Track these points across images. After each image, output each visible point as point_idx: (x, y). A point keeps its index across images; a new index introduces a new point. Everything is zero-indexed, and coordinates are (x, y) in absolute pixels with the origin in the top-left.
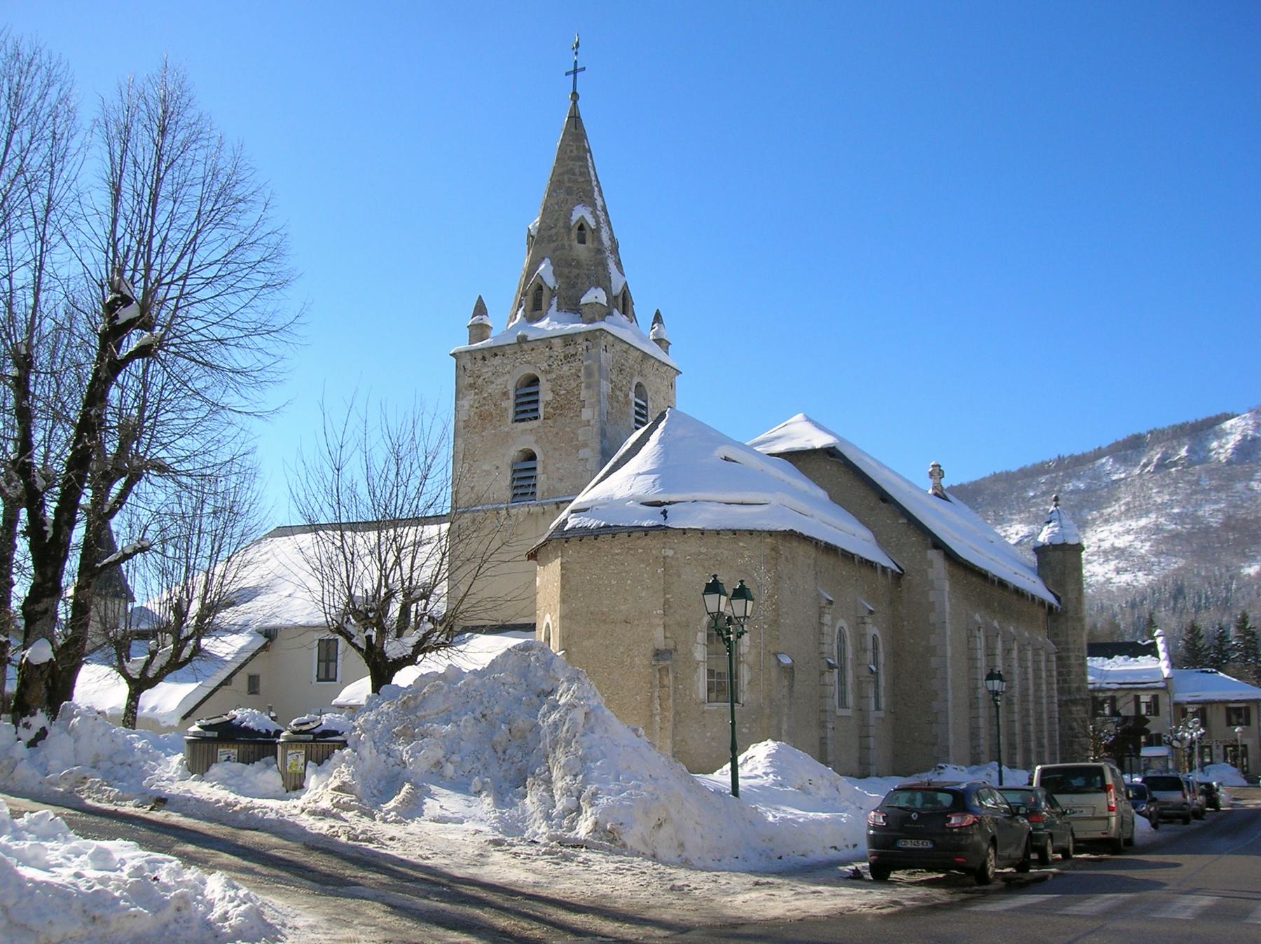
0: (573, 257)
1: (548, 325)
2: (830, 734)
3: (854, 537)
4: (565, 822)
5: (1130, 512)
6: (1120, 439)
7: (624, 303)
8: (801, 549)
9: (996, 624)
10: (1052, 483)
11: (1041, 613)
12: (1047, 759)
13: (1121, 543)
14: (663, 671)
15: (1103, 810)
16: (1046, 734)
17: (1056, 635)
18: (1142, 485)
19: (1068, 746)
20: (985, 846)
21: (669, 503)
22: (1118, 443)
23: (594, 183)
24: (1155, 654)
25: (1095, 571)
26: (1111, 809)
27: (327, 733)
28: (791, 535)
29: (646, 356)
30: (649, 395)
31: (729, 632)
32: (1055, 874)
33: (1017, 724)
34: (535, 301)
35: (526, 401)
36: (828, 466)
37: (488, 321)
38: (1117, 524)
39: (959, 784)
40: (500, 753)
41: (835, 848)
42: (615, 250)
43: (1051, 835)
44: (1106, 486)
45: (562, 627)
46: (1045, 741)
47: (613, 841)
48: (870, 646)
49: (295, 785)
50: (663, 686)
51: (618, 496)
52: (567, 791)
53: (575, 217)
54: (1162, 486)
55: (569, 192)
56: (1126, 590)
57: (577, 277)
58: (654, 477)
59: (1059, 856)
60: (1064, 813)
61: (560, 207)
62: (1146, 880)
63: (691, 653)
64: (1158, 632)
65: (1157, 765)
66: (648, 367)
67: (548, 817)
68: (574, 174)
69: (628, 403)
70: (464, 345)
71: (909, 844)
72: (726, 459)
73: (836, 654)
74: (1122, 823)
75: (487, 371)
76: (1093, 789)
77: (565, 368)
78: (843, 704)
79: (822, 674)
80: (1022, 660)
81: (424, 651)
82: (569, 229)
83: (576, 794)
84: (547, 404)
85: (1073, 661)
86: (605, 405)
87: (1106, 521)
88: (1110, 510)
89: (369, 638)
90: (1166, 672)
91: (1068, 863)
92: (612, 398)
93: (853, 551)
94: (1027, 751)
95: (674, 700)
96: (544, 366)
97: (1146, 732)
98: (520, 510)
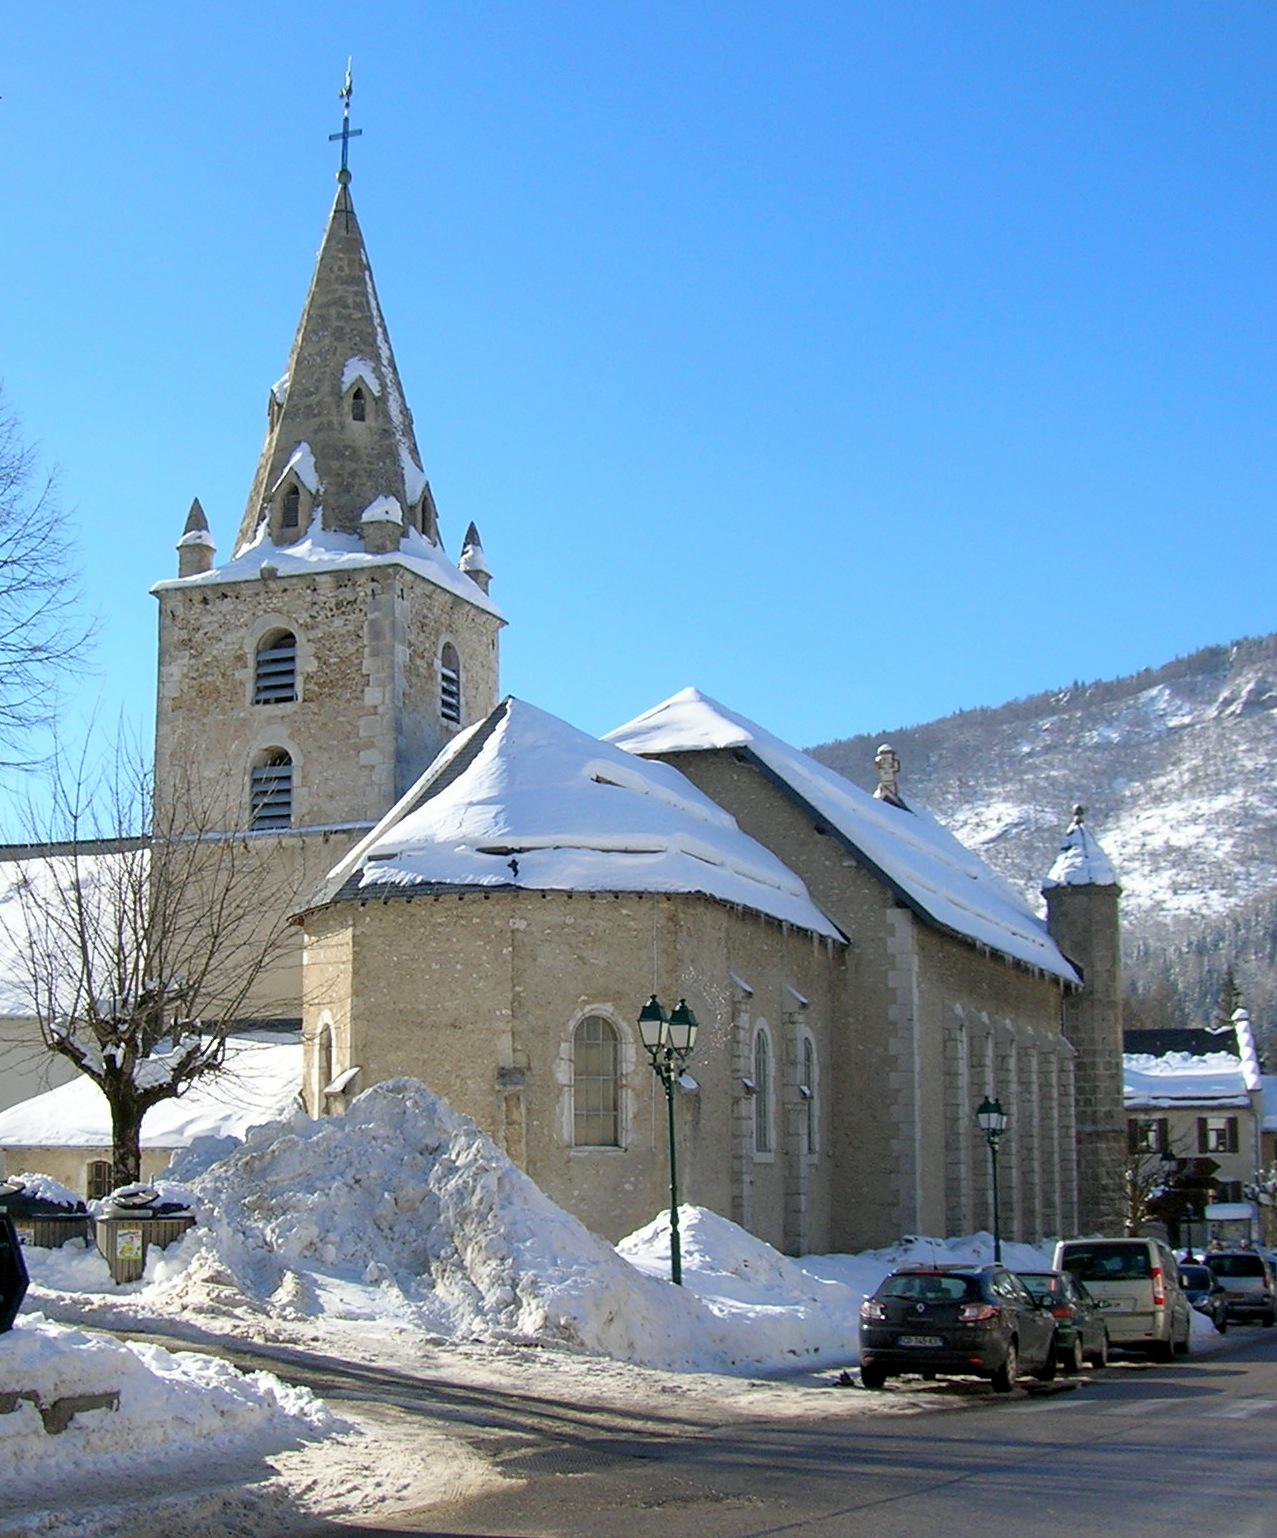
0: (344, 445)
1: (309, 553)
2: (747, 1191)
3: (773, 887)
4: (502, 1317)
5: (1197, 784)
6: (1184, 655)
7: (423, 515)
8: (709, 916)
9: (984, 1017)
10: (1061, 730)
11: (1053, 995)
12: (1076, 1231)
13: (1182, 838)
14: (512, 1100)
15: (1149, 1302)
16: (1057, 1186)
17: (1076, 1029)
18: (1221, 737)
19: (1091, 1206)
20: (1005, 1345)
21: (520, 851)
22: (1179, 662)
23: (377, 321)
24: (1234, 1050)
25: (1143, 891)
26: (1158, 1301)
27: (169, 1207)
28: (699, 897)
29: (458, 601)
30: (462, 660)
31: (668, 1070)
32: (1084, 1384)
33: (1014, 1172)
34: (287, 513)
35: (275, 676)
36: (731, 774)
37: (209, 539)
38: (1176, 805)
39: (971, 1267)
40: (387, 1231)
41: (793, 1352)
42: (408, 431)
43: (1080, 1334)
44: (1159, 738)
45: (355, 1033)
46: (1057, 1198)
47: (569, 1338)
48: (801, 1057)
49: (131, 1274)
50: (511, 1123)
51: (441, 837)
52: (497, 1280)
53: (349, 378)
54: (1254, 739)
55: (339, 335)
56: (1189, 921)
57: (353, 474)
58: (498, 808)
59: (1089, 1365)
60: (1096, 1306)
61: (324, 360)
62: (1200, 1387)
63: (551, 1074)
64: (1239, 1013)
65: (1230, 1232)
66: (460, 620)
67: (479, 1311)
68: (346, 307)
69: (431, 677)
70: (172, 580)
71: (914, 1342)
72: (598, 780)
73: (753, 1070)
74: (1172, 1320)
75: (209, 622)
76: (1132, 1273)
77: (338, 622)
78: (762, 1146)
79: (736, 1101)
80: (1022, 1070)
81: (190, 1076)
82: (339, 396)
83: (509, 1282)
84: (308, 678)
85: (1101, 1071)
86: (401, 682)
87: (1157, 800)
88: (1162, 780)
89: (110, 1059)
90: (1251, 1080)
91: (1101, 1372)
92: (410, 670)
93: (781, 917)
94: (1029, 1213)
95: (527, 1144)
96: (304, 618)
97: (1214, 1183)
98: (265, 841)
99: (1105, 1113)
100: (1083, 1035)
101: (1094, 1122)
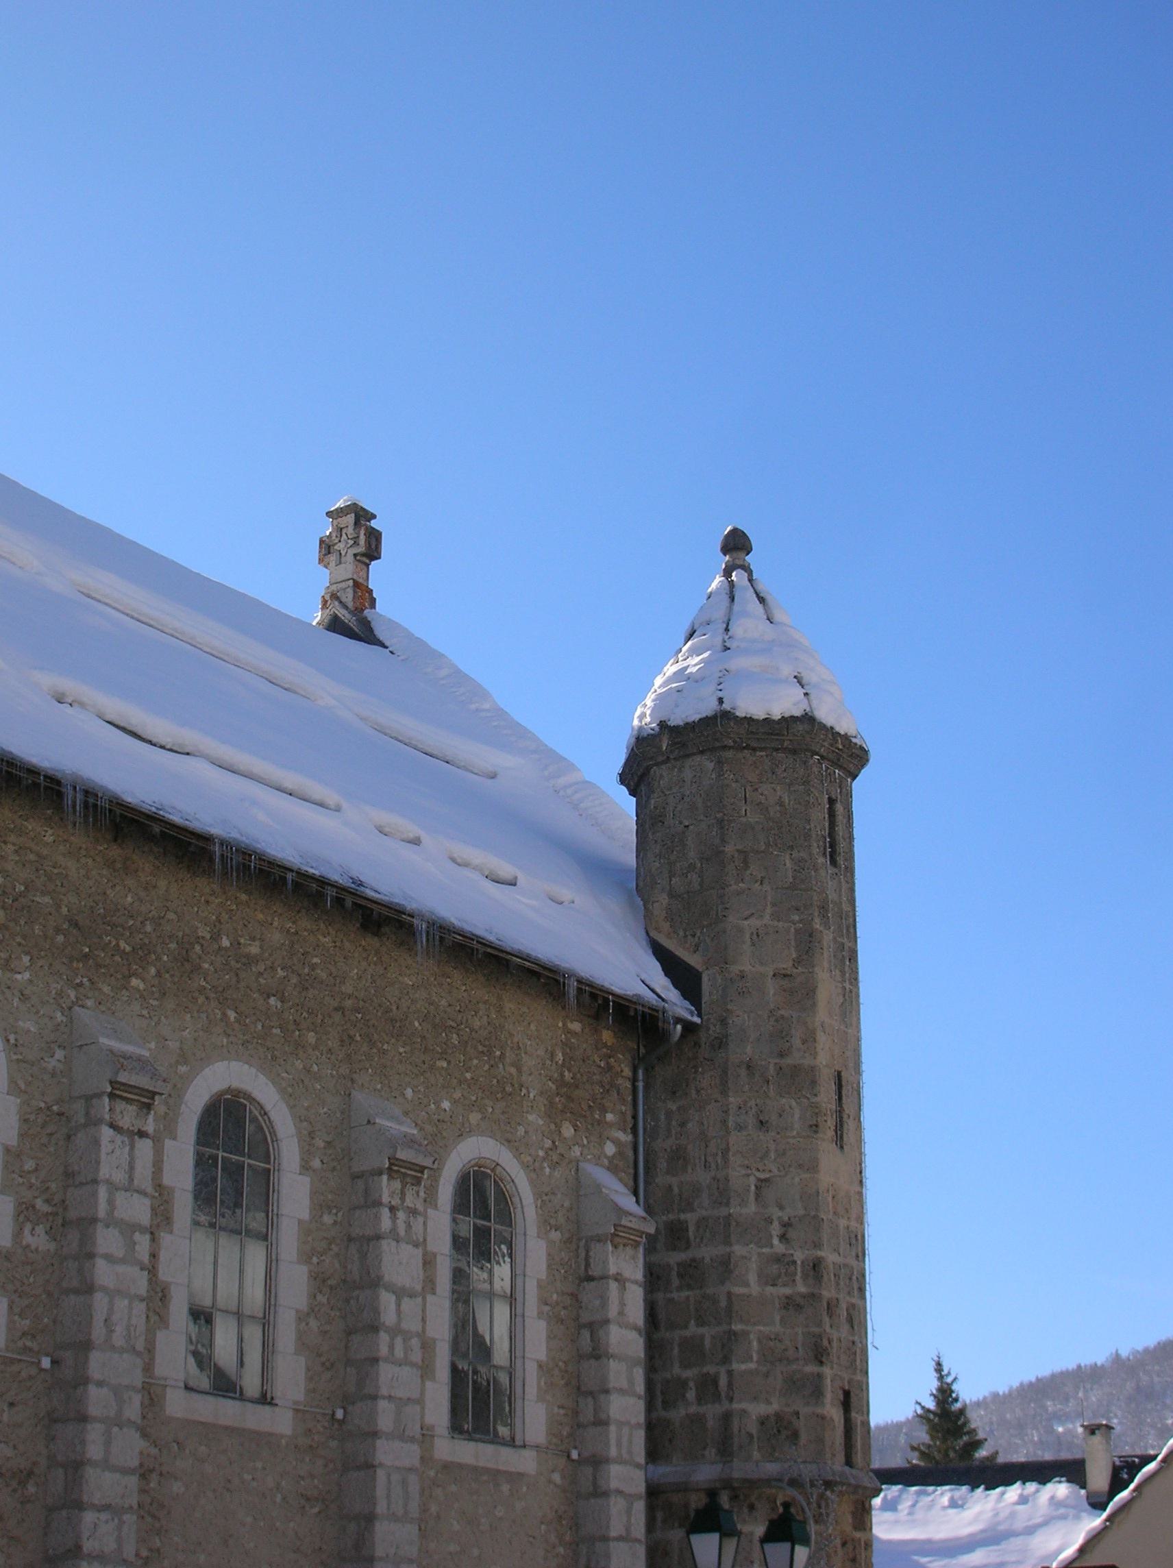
99: (763, 1422)
100: (702, 1177)
101: (725, 1450)
